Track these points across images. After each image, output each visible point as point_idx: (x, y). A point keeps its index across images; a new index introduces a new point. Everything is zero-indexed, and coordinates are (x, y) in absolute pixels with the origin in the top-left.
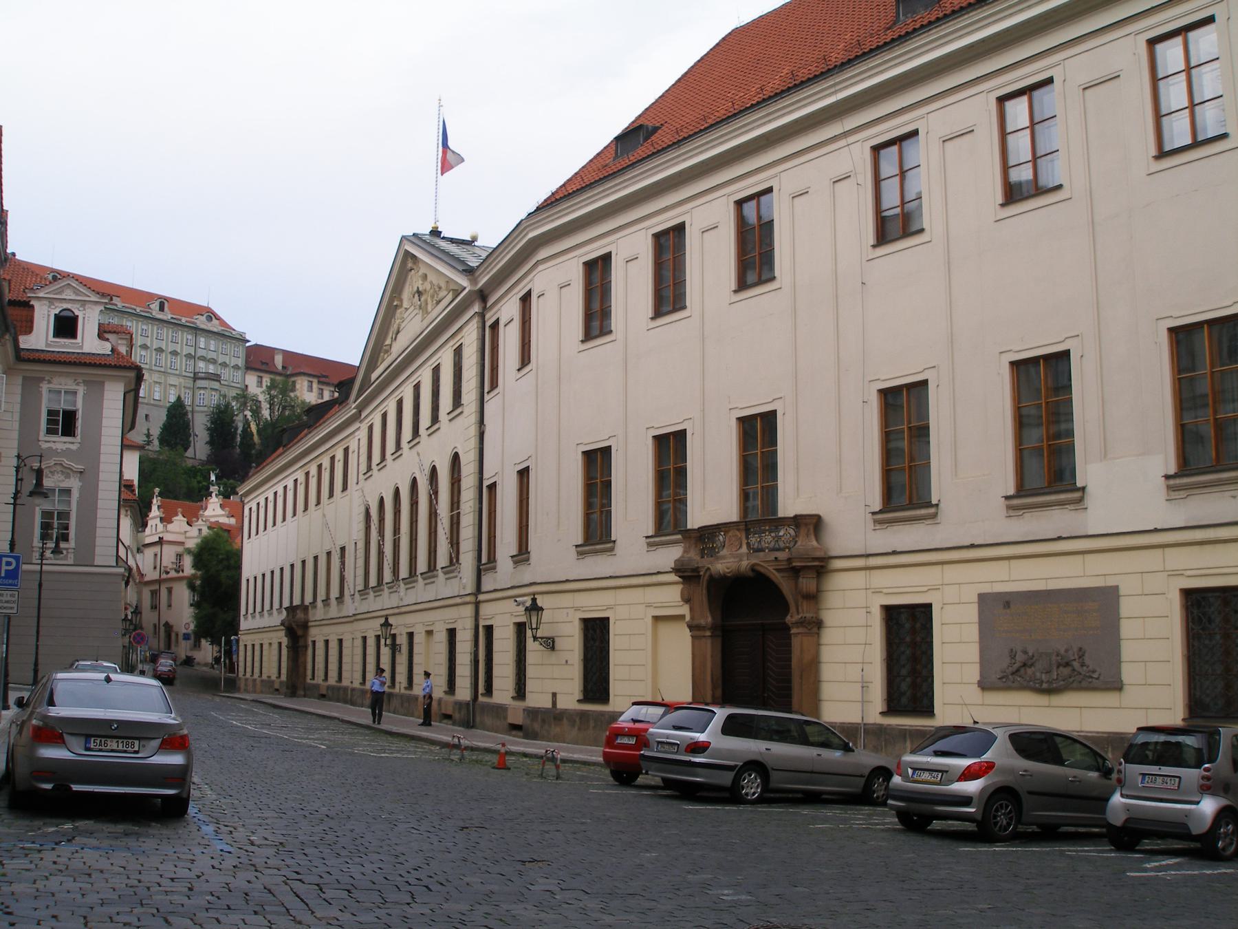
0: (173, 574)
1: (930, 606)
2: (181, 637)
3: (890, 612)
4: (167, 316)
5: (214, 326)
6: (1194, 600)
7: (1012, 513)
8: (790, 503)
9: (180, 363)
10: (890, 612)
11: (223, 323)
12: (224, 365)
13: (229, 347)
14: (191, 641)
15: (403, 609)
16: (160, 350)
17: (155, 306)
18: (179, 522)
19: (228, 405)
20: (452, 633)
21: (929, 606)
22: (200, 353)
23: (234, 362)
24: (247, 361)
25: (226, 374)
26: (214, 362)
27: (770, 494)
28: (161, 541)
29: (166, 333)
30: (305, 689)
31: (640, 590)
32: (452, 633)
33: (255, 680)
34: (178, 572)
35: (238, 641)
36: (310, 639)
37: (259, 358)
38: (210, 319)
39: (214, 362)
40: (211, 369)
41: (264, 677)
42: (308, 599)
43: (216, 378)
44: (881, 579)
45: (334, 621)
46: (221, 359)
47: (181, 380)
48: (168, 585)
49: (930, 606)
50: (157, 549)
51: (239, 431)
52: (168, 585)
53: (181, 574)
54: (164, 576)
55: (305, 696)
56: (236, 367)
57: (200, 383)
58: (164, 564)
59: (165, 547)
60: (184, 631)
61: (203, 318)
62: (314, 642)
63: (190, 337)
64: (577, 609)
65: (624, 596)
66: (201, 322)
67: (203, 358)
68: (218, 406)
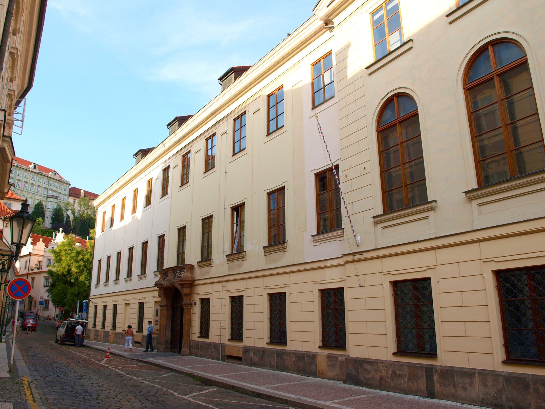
0: (36, 270)
1: (285, 293)
2: (38, 303)
3: (272, 296)
4: (37, 171)
5: (57, 177)
6: (506, 280)
7: (266, 254)
8: (187, 262)
9: (42, 191)
10: (397, 286)
11: (60, 177)
12: (60, 193)
13: (63, 186)
14: (44, 306)
15: (366, 255)
16: (33, 184)
17: (31, 166)
18: (41, 245)
19: (60, 208)
20: (141, 305)
21: (342, 289)
22: (50, 187)
23: (64, 192)
24: (69, 193)
25: (61, 197)
26: (56, 192)
27: (183, 260)
28: (30, 254)
29: (36, 177)
30: (190, 347)
31: (288, 275)
32: (141, 305)
33: (98, 331)
34: (38, 269)
35: (88, 304)
36: (197, 299)
37: (74, 192)
38: (55, 174)
39: (56, 192)
40: (55, 194)
41: (119, 329)
42: (193, 256)
43: (56, 198)
44: (318, 275)
45: (223, 280)
46: (59, 191)
47: (41, 197)
48: (33, 276)
49: (285, 293)
50: (28, 258)
51: (65, 219)
52: (33, 276)
53: (40, 270)
54: (31, 272)
55: (190, 354)
56: (65, 195)
57: (49, 199)
58: (30, 265)
59: (32, 257)
60: (40, 300)
61: (53, 174)
62: (206, 303)
63: (46, 180)
64: (387, 274)
65: (295, 278)
66: (50, 174)
67: (51, 190)
68: (56, 208)
